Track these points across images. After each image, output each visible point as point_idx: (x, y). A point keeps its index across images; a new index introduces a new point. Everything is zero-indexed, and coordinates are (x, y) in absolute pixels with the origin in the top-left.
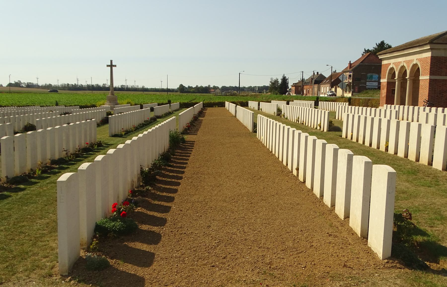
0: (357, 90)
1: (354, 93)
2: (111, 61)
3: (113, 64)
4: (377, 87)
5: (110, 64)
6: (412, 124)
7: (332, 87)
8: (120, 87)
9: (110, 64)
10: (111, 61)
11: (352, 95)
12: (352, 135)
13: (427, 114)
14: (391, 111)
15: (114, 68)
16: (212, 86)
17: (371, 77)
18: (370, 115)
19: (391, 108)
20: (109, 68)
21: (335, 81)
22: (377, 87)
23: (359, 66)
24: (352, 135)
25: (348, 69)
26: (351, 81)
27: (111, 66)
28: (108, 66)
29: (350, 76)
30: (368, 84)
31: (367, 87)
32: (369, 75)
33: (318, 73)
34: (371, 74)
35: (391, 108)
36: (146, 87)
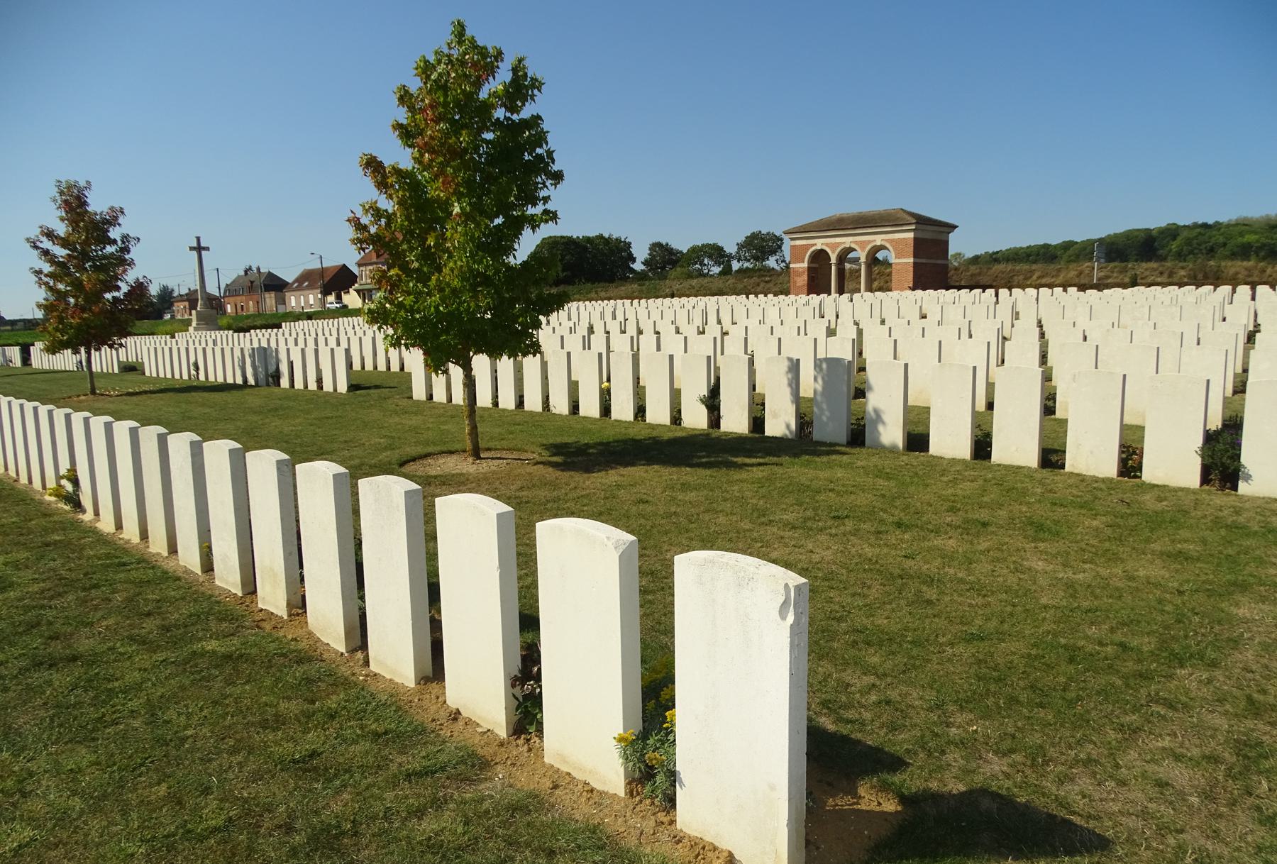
2: (198, 239)
7: (326, 293)
10: (198, 239)
14: (288, 350)
25: (375, 260)
27: (199, 249)
28: (192, 249)
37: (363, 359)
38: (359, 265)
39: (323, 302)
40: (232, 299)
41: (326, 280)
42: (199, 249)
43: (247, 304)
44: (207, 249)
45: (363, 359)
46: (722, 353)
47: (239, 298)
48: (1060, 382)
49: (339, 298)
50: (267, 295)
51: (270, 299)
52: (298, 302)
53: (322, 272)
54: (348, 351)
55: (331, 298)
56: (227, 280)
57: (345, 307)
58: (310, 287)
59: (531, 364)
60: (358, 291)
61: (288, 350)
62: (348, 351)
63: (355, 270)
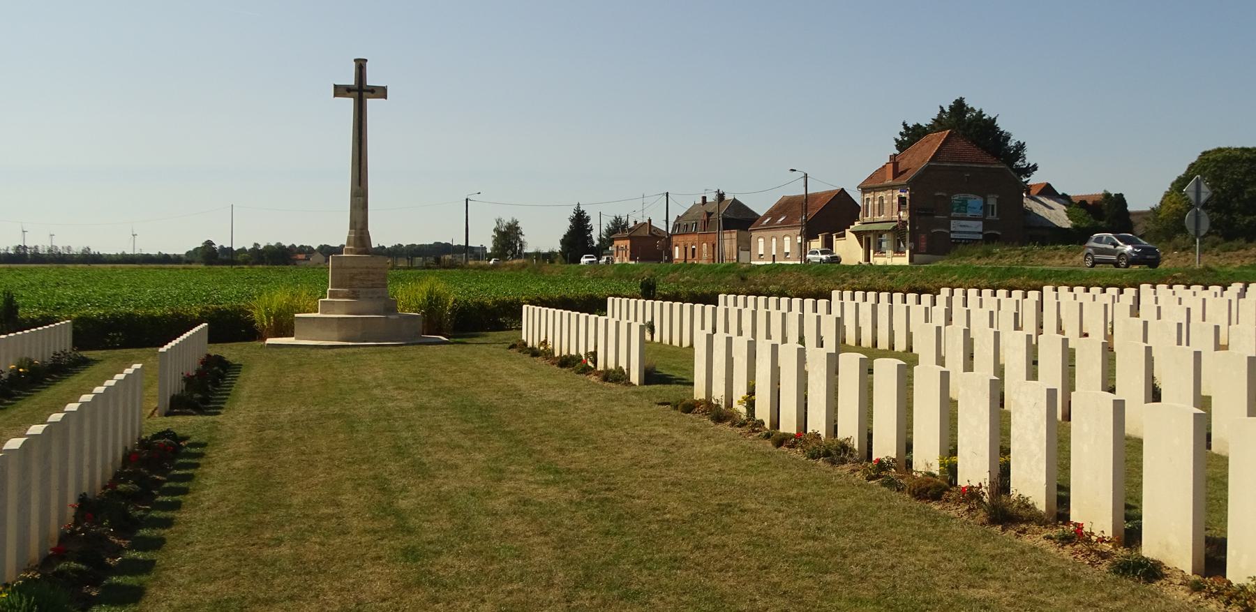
0: (923, 244)
1: (916, 257)
2: (361, 65)
3: (371, 81)
4: (981, 237)
5: (351, 81)
6: (782, 348)
7: (809, 235)
8: (11, 252)
9: (351, 81)
10: (361, 65)
11: (911, 260)
12: (751, 392)
13: (784, 315)
14: (768, 314)
15: (372, 104)
16: (522, 238)
17: (964, 203)
18: (703, 328)
19: (767, 306)
20: (349, 103)
21: (829, 215)
22: (981, 237)
23: (927, 170)
24: (751, 392)
25: (889, 181)
26: (904, 215)
27: (360, 91)
28: (340, 91)
29: (902, 200)
30: (954, 225)
31: (952, 236)
32: (956, 197)
33: (721, 197)
34: (962, 196)
35: (767, 306)
36: (94, 250)
37: (858, 330)
38: (864, 189)
39: (803, 249)
40: (681, 238)
41: (812, 213)
42: (360, 91)
43: (700, 248)
44: (381, 92)
45: (858, 330)
46: (1106, 306)
47: (690, 238)
48: (1063, 316)
49: (828, 244)
50: (727, 236)
51: (729, 241)
52: (768, 248)
53: (807, 200)
54: (840, 322)
55: (816, 244)
56: (677, 211)
57: (836, 260)
58: (787, 225)
59: (602, 319)
60: (858, 234)
61: (768, 314)
62: (840, 322)
63: (857, 197)
